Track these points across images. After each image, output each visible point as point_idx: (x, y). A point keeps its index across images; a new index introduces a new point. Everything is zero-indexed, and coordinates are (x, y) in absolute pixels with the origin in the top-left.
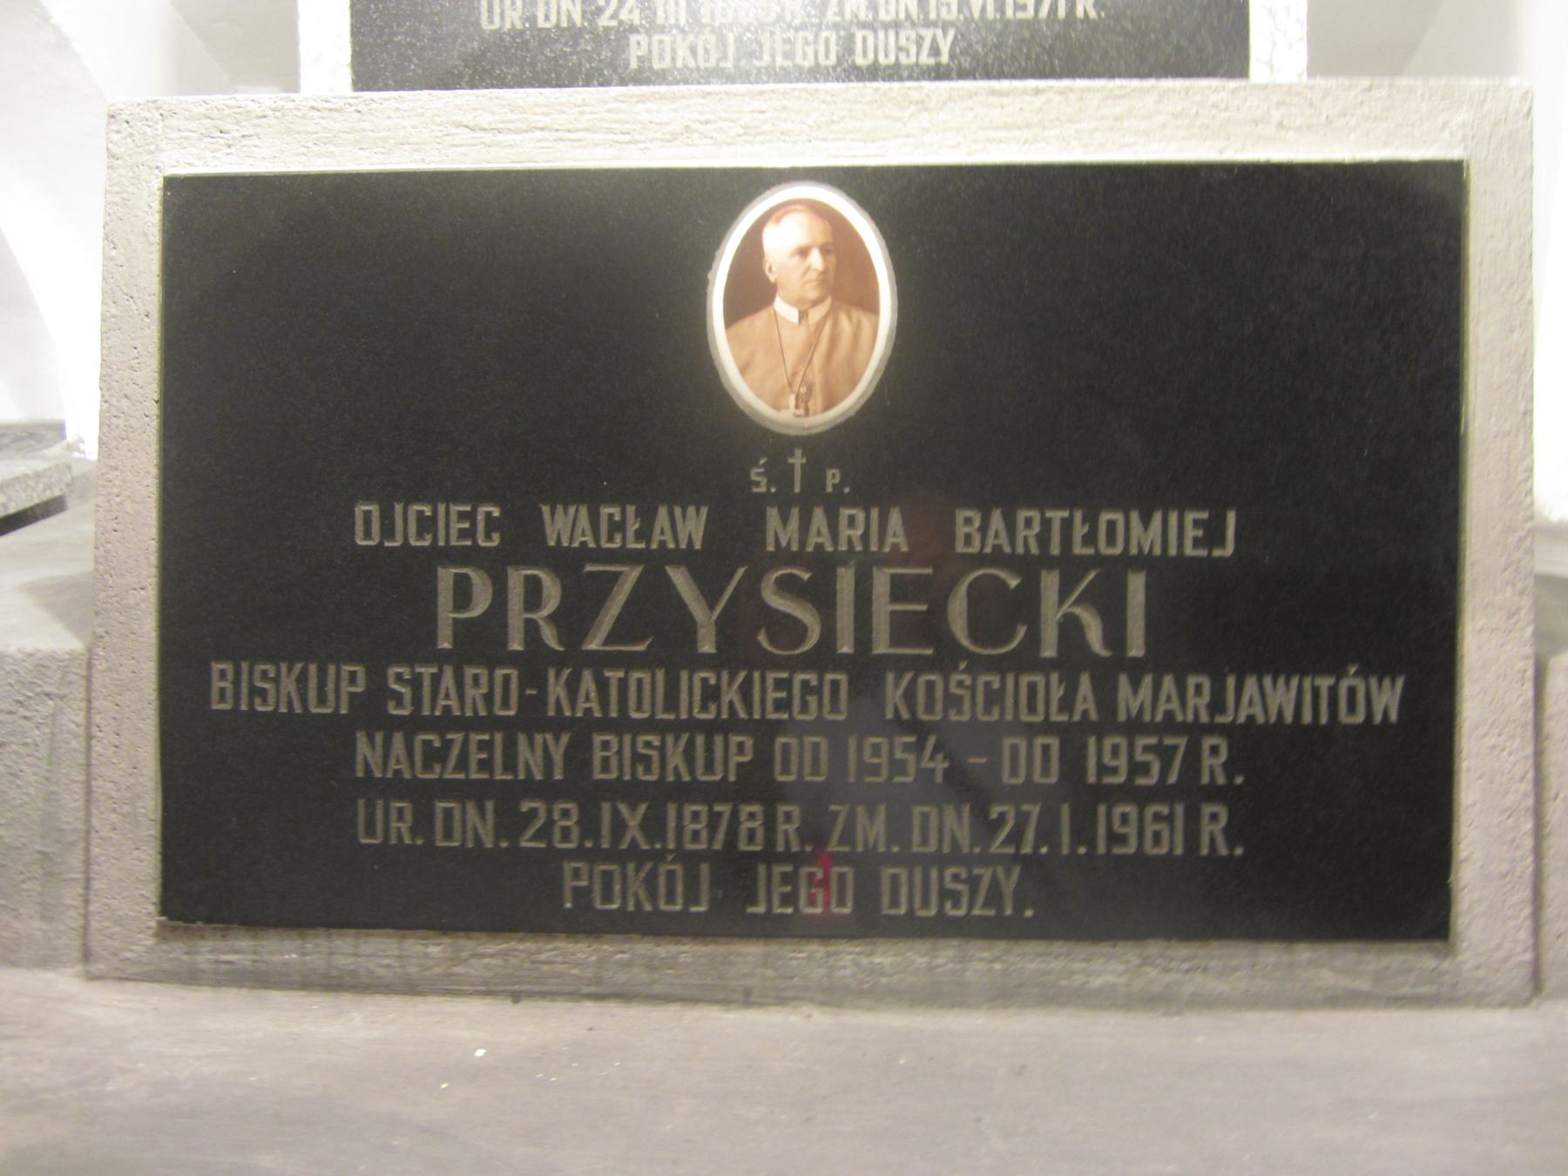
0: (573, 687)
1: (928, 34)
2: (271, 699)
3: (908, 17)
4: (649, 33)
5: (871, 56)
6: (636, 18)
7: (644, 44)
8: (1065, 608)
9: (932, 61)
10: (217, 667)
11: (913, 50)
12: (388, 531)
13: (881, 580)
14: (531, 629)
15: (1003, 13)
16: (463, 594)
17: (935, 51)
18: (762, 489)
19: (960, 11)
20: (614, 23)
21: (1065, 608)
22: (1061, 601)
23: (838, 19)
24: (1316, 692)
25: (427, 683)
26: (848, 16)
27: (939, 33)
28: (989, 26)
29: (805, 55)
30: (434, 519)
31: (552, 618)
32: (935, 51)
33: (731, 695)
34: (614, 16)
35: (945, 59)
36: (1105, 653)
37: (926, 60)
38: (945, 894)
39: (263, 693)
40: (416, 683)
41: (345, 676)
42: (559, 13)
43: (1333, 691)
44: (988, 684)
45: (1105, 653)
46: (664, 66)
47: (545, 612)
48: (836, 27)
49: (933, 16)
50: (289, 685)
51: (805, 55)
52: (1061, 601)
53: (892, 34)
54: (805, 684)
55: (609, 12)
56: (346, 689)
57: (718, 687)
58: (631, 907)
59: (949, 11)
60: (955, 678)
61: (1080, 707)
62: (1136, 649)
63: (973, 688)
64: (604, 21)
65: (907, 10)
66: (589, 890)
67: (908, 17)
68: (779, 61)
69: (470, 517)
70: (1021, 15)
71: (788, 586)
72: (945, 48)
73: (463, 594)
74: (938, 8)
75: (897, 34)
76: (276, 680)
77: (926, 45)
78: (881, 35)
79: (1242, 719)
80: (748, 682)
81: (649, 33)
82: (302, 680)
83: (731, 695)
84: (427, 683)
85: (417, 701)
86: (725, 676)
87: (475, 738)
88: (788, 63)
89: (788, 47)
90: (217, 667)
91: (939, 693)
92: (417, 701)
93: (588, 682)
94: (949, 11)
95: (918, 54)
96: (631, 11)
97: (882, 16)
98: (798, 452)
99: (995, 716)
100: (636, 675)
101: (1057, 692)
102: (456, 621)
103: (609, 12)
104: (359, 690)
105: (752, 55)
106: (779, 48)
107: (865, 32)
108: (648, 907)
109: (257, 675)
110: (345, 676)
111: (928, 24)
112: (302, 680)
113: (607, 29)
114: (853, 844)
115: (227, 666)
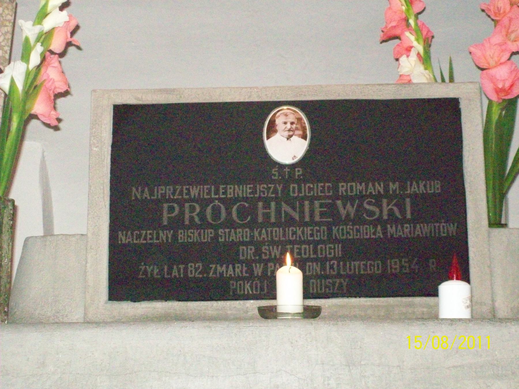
0: (260, 234)
8: (390, 207)
10: (180, 231)
12: (300, 191)
13: (317, 203)
14: (192, 219)
16: (171, 209)
18: (276, 178)
21: (390, 207)
22: (388, 206)
24: (435, 227)
25: (269, 232)
30: (313, 188)
31: (198, 215)
36: (199, 223)
38: (326, 287)
39: (190, 237)
41: (209, 233)
43: (439, 227)
44: (292, 230)
45: (199, 223)
47: (195, 213)
50: (196, 234)
52: (388, 206)
54: (357, 228)
57: (296, 232)
58: (246, 293)
60: (348, 227)
62: (409, 216)
63: (353, 229)
66: (236, 289)
69: (323, 187)
71: (369, 203)
73: (171, 209)
79: (416, 236)
80: (303, 230)
84: (269, 232)
86: (298, 228)
87: (296, 246)
90: (180, 231)
91: (345, 231)
98: (287, 168)
99: (294, 238)
100: (275, 229)
102: (169, 218)
104: (212, 235)
108: (251, 292)
110: (209, 233)
112: (200, 234)
114: (147, 275)
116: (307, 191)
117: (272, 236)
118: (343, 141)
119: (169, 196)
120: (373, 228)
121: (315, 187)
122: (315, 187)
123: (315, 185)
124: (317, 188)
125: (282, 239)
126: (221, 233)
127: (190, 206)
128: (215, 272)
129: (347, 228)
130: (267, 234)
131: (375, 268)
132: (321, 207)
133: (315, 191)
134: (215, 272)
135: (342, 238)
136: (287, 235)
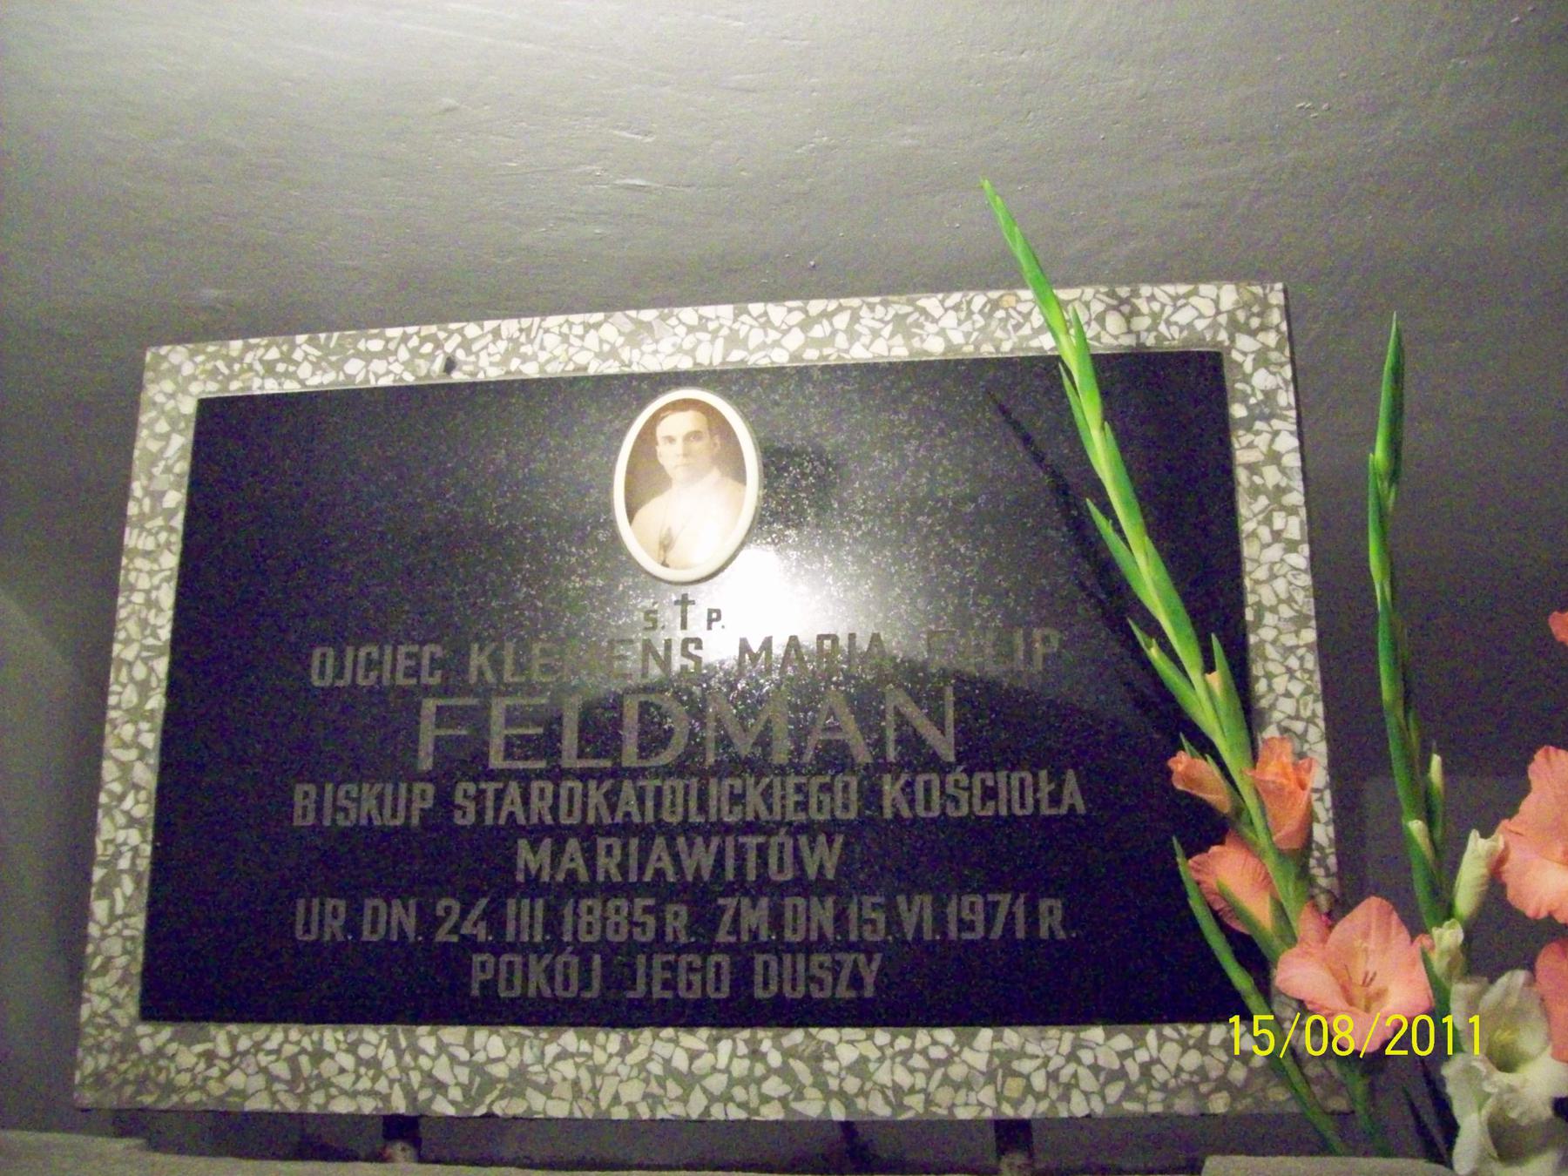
1: (848, 959)
2: (353, 816)
3: (822, 936)
4: (497, 954)
5: (774, 988)
6: (482, 933)
7: (490, 966)
9: (852, 994)
11: (829, 979)
15: (945, 934)
17: (856, 981)
19: (888, 931)
20: (455, 939)
23: (732, 939)
26: (745, 938)
27: (862, 958)
28: (929, 948)
29: (689, 986)
32: (856, 981)
33: (754, 798)
34: (455, 929)
35: (869, 992)
37: (844, 993)
40: (480, 796)
42: (388, 923)
46: (513, 994)
48: (728, 949)
49: (853, 937)
51: (689, 986)
53: (801, 958)
55: (448, 925)
56: (417, 805)
57: (743, 795)
59: (874, 931)
61: (1067, 801)
63: (969, 789)
64: (442, 936)
65: (820, 928)
67: (822, 936)
68: (658, 993)
70: (967, 936)
72: (869, 975)
74: (860, 927)
75: (808, 961)
76: (358, 800)
77: (845, 974)
78: (787, 959)
81: (497, 954)
82: (380, 798)
83: (754, 798)
84: (490, 795)
85: (480, 813)
88: (668, 995)
89: (668, 975)
92: (480, 813)
93: (628, 788)
94: (874, 931)
95: (835, 985)
96: (475, 924)
97: (789, 935)
101: (1046, 788)
103: (448, 925)
105: (620, 986)
106: (659, 975)
107: (765, 957)
109: (341, 794)
111: (851, 947)
112: (380, 798)
113: (446, 945)
115: (311, 788)
116: (361, 672)
117: (658, 806)
118: (1195, 526)
119: (481, 673)
120: (1050, 781)
121: (388, 658)
122: (388, 658)
123: (388, 650)
124: (395, 659)
125: (696, 819)
126: (466, 796)
127: (439, 709)
128: (735, 929)
129: (943, 784)
130: (641, 801)
131: (976, 915)
132: (510, 722)
133: (387, 667)
134: (735, 929)
135: (392, 823)
136: (713, 803)
